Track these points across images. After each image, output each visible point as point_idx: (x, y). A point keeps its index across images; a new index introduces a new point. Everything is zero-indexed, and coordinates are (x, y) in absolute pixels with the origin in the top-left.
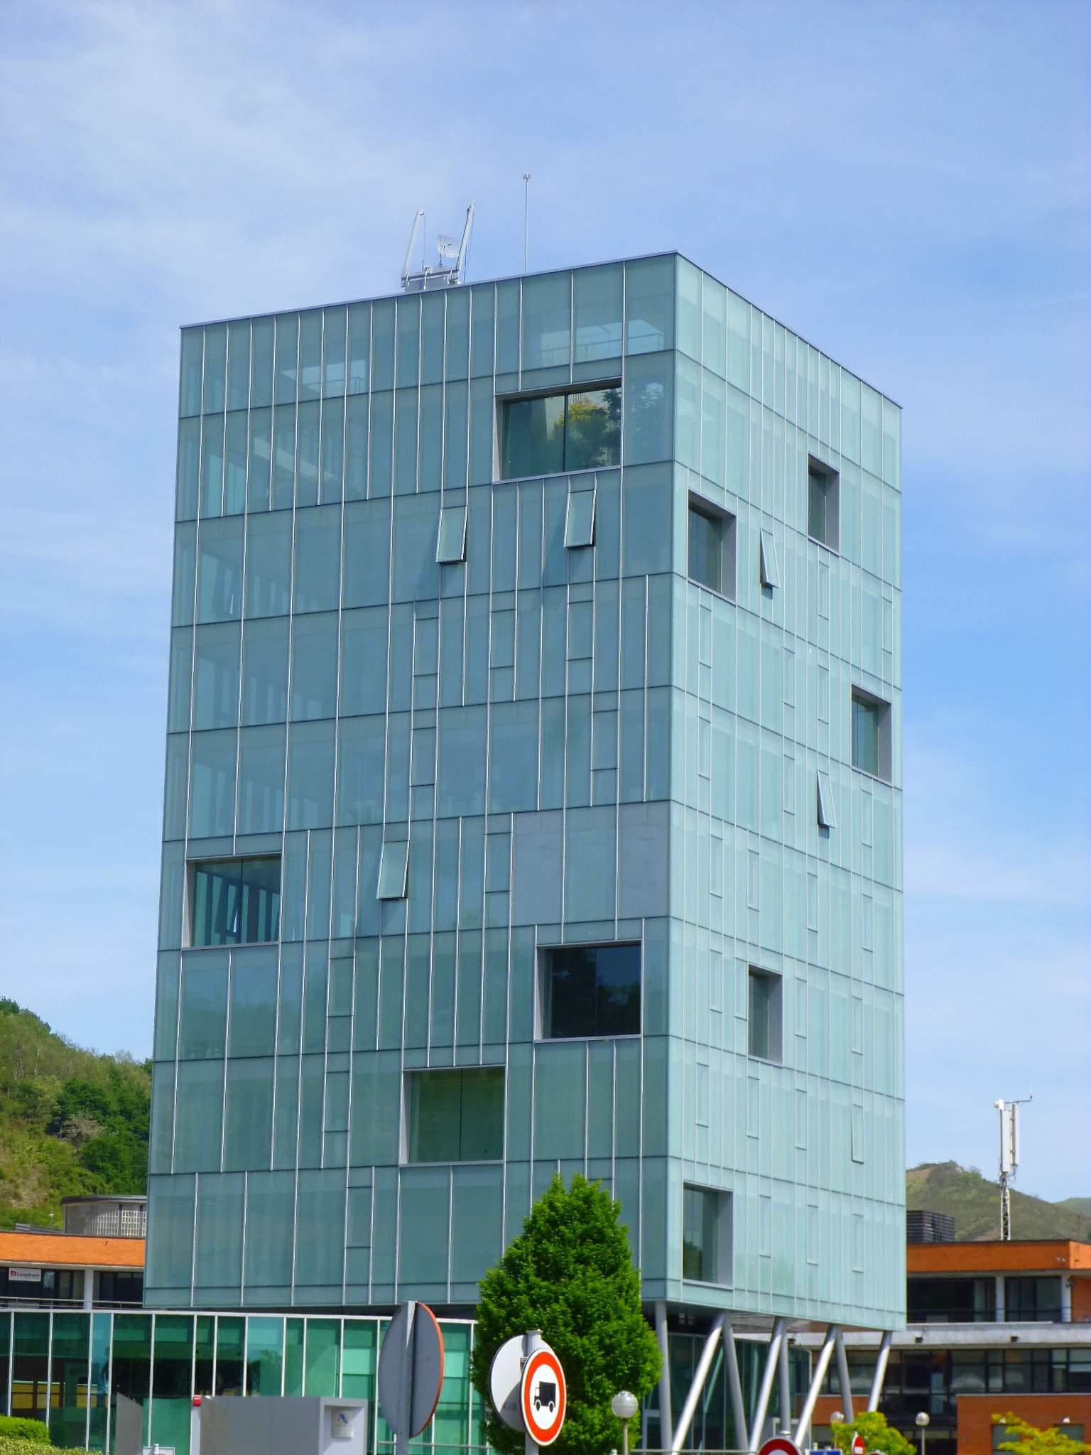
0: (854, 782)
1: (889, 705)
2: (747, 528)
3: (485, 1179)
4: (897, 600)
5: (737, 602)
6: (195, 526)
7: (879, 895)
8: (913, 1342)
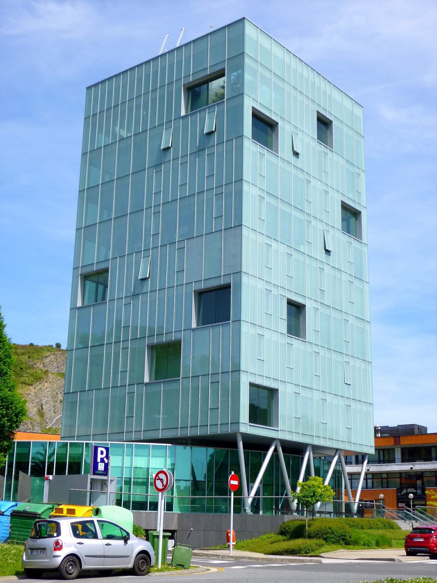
0: (344, 238)
1: (360, 212)
2: (284, 131)
3: (173, 386)
4: (363, 176)
5: (279, 155)
6: (90, 155)
7: (356, 283)
8: (409, 469)
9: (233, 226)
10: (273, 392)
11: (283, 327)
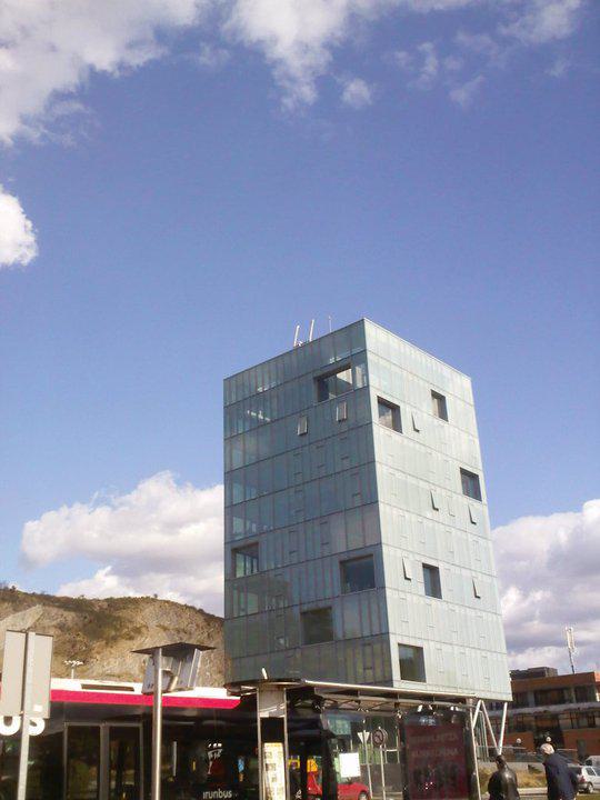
7: (481, 541)
9: (371, 502)
10: (419, 650)
11: (421, 589)
